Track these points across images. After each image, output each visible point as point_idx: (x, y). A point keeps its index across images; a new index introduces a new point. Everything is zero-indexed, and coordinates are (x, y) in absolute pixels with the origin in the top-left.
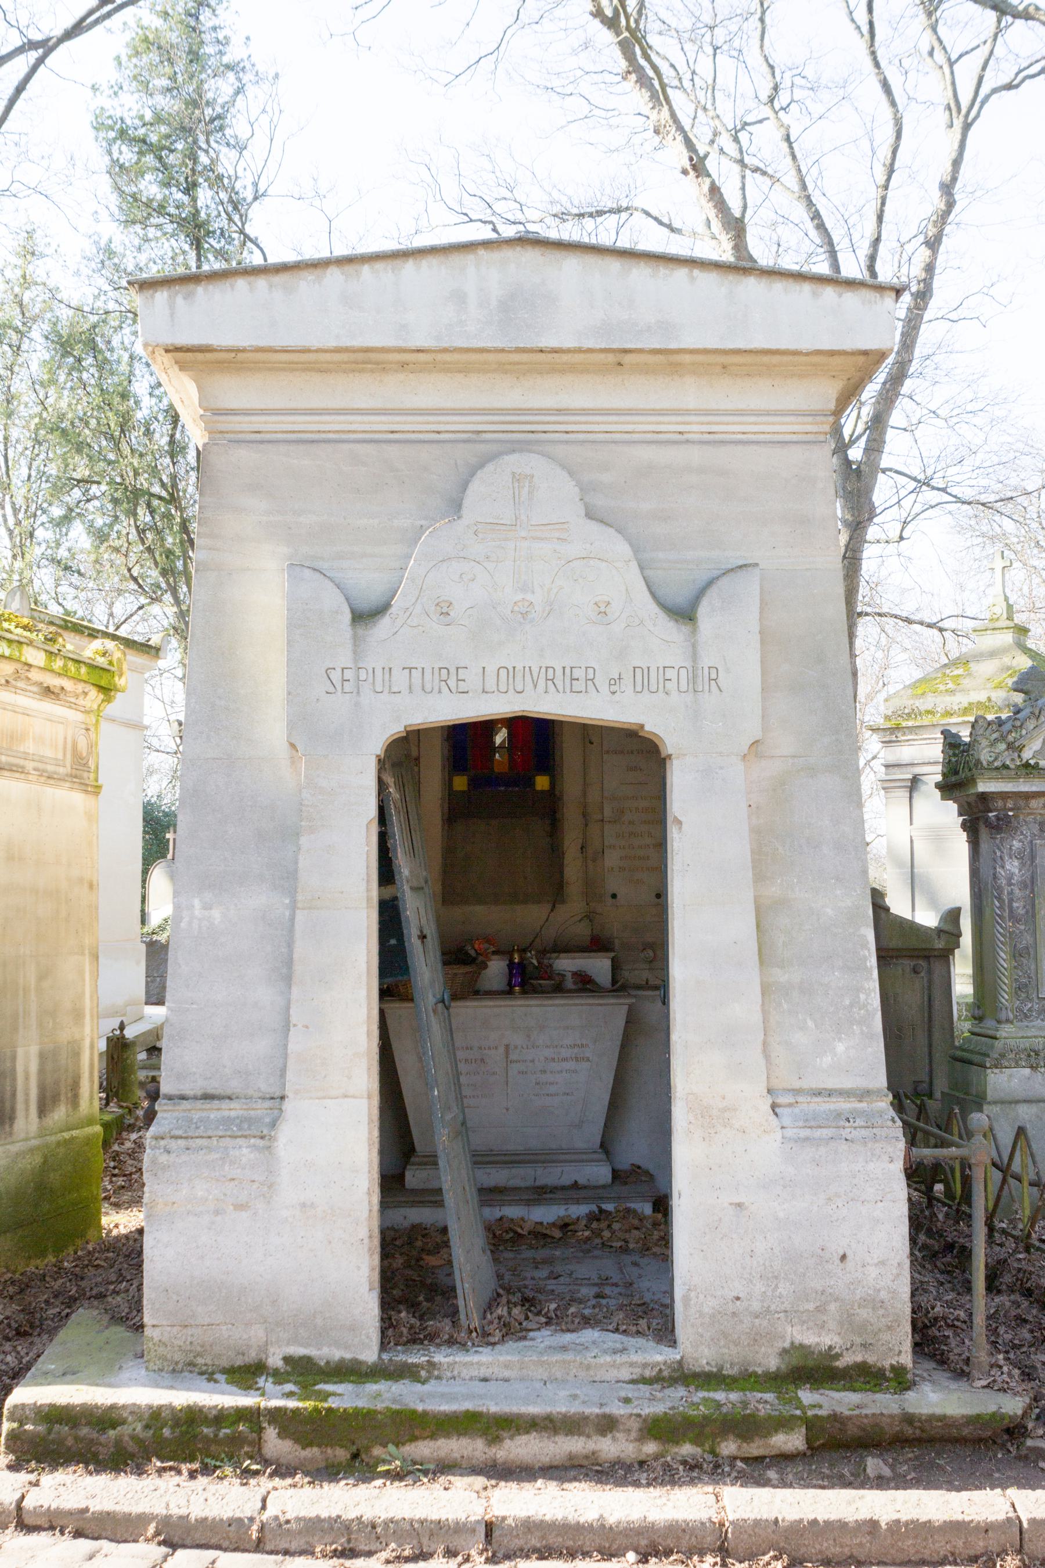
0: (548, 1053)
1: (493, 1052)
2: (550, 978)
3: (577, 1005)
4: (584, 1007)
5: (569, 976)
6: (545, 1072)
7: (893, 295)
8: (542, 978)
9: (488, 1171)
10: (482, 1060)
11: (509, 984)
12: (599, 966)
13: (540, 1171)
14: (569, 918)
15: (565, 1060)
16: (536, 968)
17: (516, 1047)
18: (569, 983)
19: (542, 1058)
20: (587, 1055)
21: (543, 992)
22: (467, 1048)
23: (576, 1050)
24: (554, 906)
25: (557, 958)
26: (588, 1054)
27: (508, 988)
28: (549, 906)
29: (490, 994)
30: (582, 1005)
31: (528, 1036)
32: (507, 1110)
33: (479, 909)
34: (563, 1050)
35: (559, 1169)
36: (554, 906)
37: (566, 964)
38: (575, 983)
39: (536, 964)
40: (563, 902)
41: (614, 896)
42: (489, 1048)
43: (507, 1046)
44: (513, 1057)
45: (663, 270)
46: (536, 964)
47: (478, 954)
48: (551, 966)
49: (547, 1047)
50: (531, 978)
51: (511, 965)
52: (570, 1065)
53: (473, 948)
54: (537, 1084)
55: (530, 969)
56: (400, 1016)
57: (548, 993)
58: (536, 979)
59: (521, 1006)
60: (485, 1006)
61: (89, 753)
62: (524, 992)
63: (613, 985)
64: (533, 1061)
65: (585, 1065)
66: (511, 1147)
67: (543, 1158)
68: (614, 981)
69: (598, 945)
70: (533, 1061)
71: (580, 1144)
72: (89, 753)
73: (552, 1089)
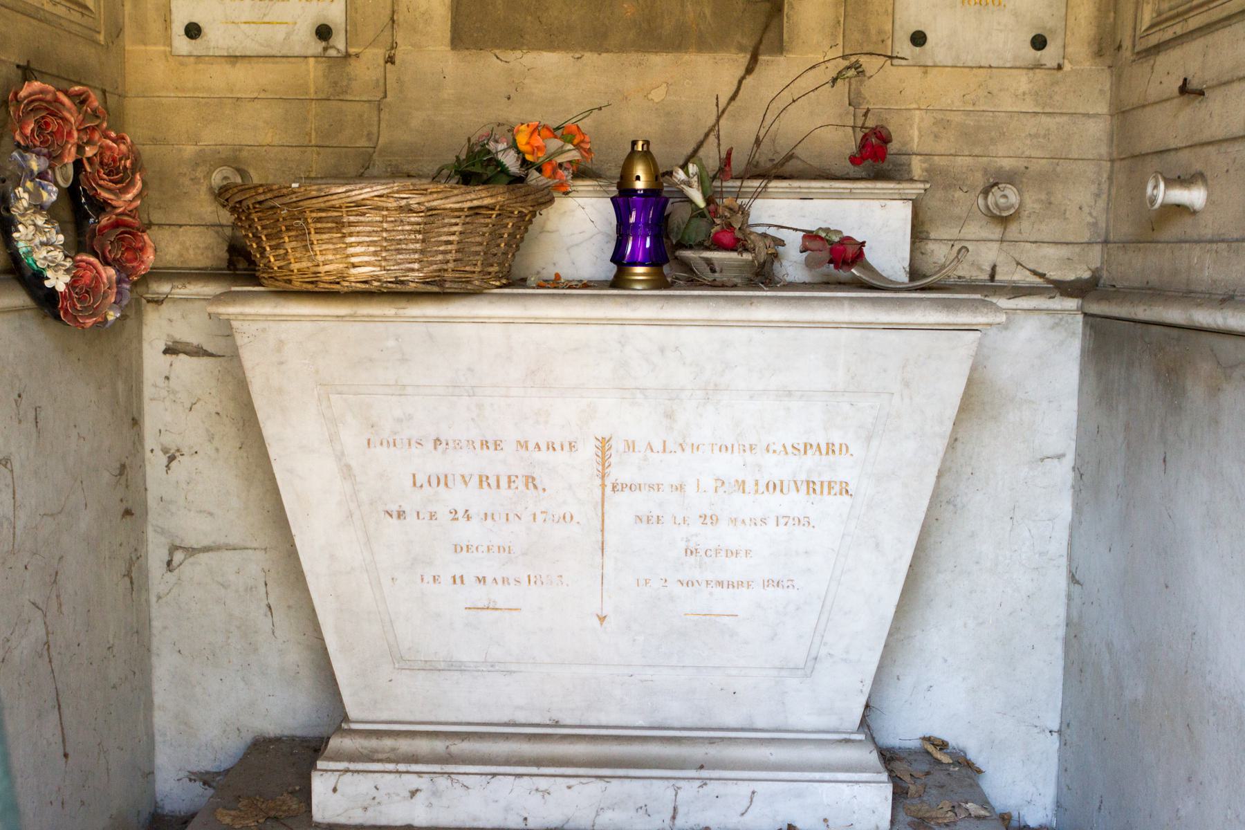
0: (729, 466)
1: (561, 457)
2: (738, 245)
3: (823, 325)
4: (845, 334)
5: (794, 241)
6: (714, 520)
7: (1189, 87)
8: (719, 245)
9: (543, 783)
10: (530, 481)
11: (617, 257)
12: (878, 221)
13: (689, 790)
14: (796, 94)
15: (775, 487)
16: (700, 214)
17: (631, 446)
18: (793, 264)
19: (708, 482)
20: (842, 475)
21: (714, 285)
22: (485, 444)
23: (811, 459)
24: (754, 59)
25: (756, 195)
26: (844, 468)
27: (613, 268)
28: (744, 59)
29: (556, 285)
30: (837, 326)
31: (669, 415)
32: (602, 619)
33: (550, 61)
34: (771, 459)
35: (745, 789)
36: (754, 59)
37: (783, 212)
38: (809, 264)
39: (701, 203)
40: (779, 48)
41: (918, 39)
42: (551, 447)
43: (604, 445)
44: (617, 473)
45: (578, 723)
46: (701, 203)
47: (524, 163)
48: (744, 211)
49: (724, 448)
50: (682, 245)
51: (624, 200)
52: (794, 503)
53: (514, 145)
54: (690, 552)
55: (678, 214)
56: (281, 344)
57: (734, 287)
58: (702, 246)
59: (650, 323)
60: (537, 322)
61: (242, 172)
62: (660, 282)
63: (912, 279)
64: (680, 488)
65: (834, 503)
66: (610, 716)
67: (698, 752)
68: (914, 273)
69: (874, 157)
70: (680, 488)
71: (804, 713)
72: (242, 172)
73: (734, 569)
